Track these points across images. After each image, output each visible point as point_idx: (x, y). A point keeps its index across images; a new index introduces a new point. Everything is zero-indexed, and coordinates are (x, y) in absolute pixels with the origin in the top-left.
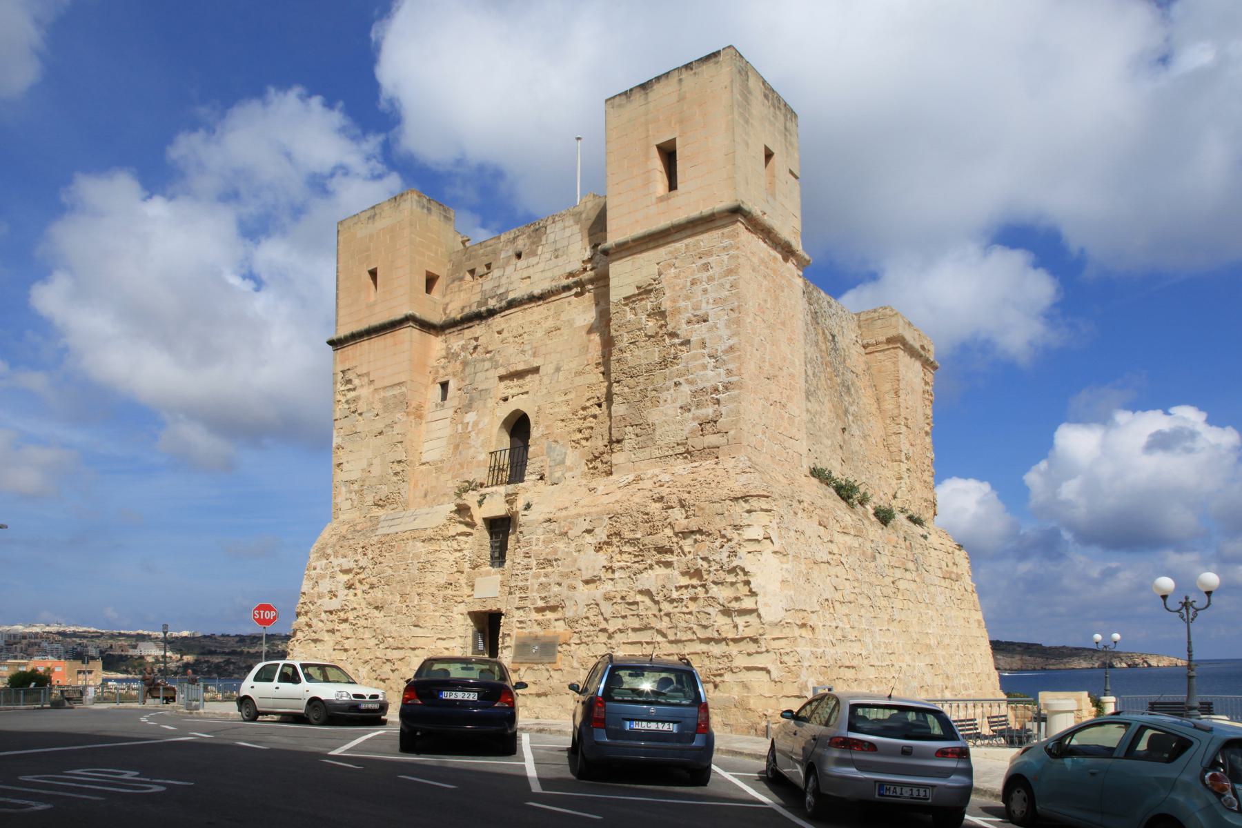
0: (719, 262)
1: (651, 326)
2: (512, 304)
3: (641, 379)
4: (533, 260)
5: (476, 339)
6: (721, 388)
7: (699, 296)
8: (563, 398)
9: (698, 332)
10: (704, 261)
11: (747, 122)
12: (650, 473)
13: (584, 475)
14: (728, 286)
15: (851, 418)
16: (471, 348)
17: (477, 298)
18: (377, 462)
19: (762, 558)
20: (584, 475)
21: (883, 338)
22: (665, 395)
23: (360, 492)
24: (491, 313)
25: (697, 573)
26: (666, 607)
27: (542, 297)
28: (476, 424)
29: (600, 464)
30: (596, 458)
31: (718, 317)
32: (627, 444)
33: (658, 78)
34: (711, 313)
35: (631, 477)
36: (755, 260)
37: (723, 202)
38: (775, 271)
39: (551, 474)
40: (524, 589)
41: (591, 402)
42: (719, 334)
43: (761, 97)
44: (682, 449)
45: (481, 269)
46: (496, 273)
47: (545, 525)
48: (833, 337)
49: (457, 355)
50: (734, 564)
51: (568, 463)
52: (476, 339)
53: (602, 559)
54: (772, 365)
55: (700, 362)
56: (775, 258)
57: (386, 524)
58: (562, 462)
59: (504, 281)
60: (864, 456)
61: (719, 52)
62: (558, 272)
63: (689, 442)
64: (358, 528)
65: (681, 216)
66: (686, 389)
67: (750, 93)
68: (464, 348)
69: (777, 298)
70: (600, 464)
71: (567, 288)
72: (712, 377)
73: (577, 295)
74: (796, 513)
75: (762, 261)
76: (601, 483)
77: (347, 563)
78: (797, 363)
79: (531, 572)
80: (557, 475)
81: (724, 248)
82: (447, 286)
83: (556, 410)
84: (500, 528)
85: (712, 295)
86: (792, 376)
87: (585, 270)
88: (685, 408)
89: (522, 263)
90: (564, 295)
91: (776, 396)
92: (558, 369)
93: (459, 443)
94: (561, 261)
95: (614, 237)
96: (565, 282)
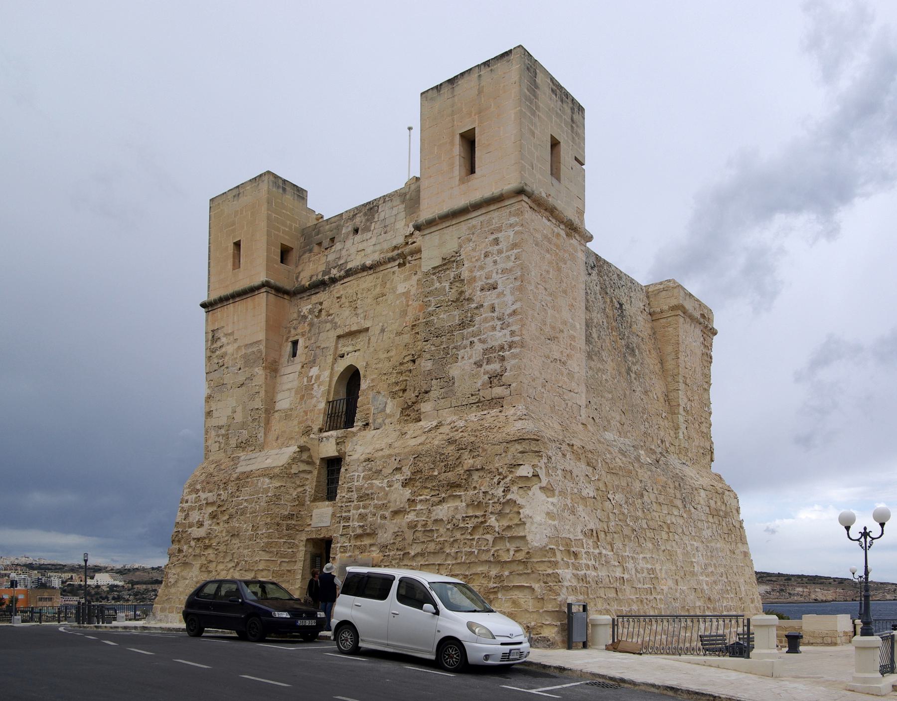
0: (507, 236)
2: (349, 273)
3: (444, 339)
4: (369, 234)
5: (321, 304)
6: (506, 347)
7: (490, 267)
8: (385, 355)
9: (490, 298)
10: (494, 236)
11: (534, 114)
12: (449, 420)
13: (399, 421)
14: (513, 258)
15: (633, 375)
16: (317, 311)
17: (322, 268)
18: (239, 409)
19: (530, 493)
20: (399, 421)
21: (666, 307)
22: (461, 353)
23: (226, 437)
24: (334, 281)
27: (371, 268)
28: (318, 377)
29: (410, 412)
30: (409, 407)
31: (505, 285)
32: (433, 394)
33: (462, 74)
34: (500, 282)
35: (435, 423)
36: (539, 236)
37: (512, 184)
38: (557, 246)
39: (374, 420)
40: (347, 519)
41: (407, 359)
42: (506, 299)
43: (548, 91)
44: (474, 399)
45: (326, 243)
46: (338, 246)
47: (365, 464)
48: (621, 305)
49: (305, 317)
50: (508, 497)
51: (388, 411)
52: (321, 304)
53: (407, 493)
54: (553, 328)
55: (490, 324)
56: (558, 235)
57: (244, 463)
58: (384, 410)
59: (344, 253)
60: (644, 409)
61: (510, 51)
62: (386, 246)
63: (481, 393)
64: (222, 467)
65: (477, 196)
66: (479, 347)
67: (537, 87)
68: (311, 311)
69: (559, 270)
70: (410, 412)
71: (392, 259)
72: (500, 337)
73: (400, 265)
74: (564, 455)
75: (545, 237)
76: (412, 429)
77: (211, 497)
78: (578, 326)
79: (353, 504)
80: (380, 421)
81: (511, 225)
82: (300, 257)
83: (380, 365)
84: (333, 465)
85: (501, 266)
86: (573, 338)
87: (407, 243)
88: (478, 364)
89: (358, 237)
90: (389, 265)
91: (557, 355)
92: (383, 331)
94: (388, 236)
95: (426, 213)
96: (390, 255)
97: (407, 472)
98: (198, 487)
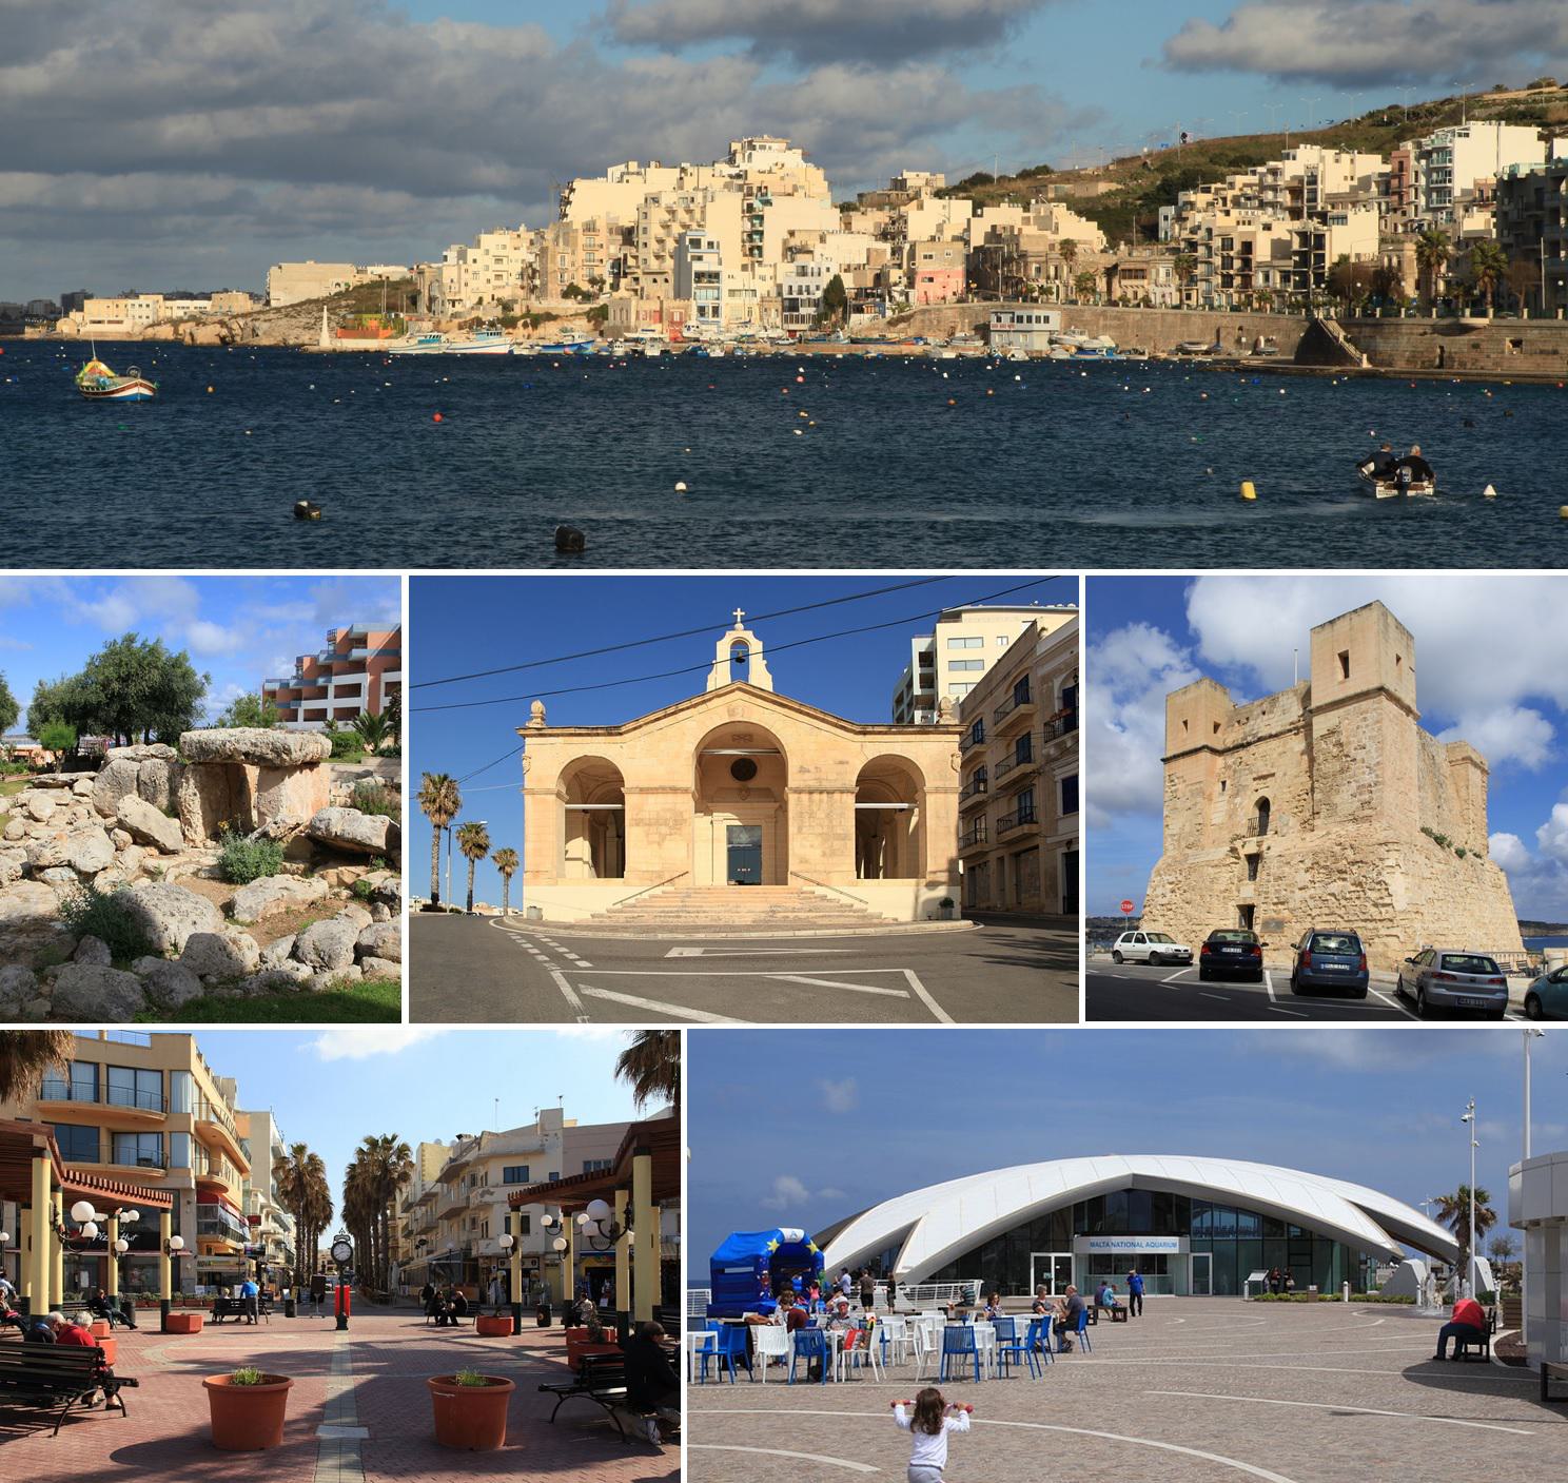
1: (1335, 751)
9: (1360, 755)
25: (1360, 884)
26: (1343, 902)
46: (1251, 722)
53: (1308, 876)
88: (1353, 796)
93: (1231, 814)
97: (1308, 863)
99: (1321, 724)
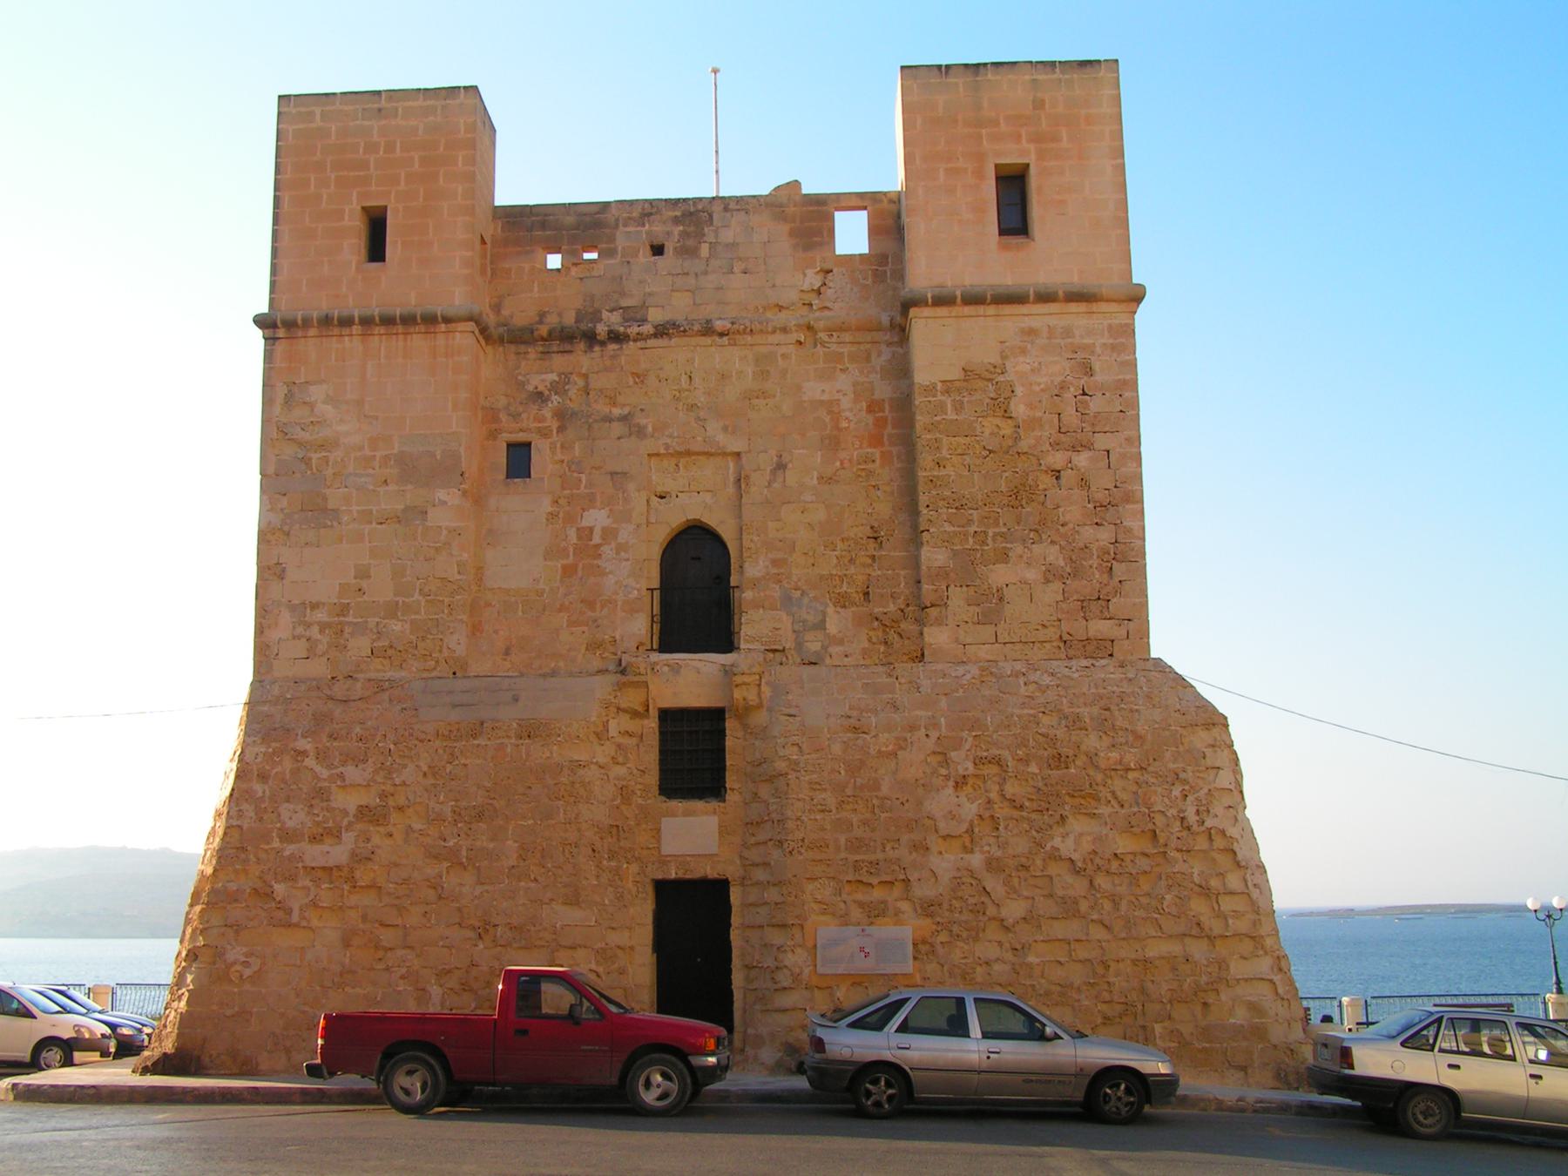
28: (609, 534)
58: (821, 625)
89: (667, 262)
92: (781, 467)
98: (303, 744)
99: (938, 347)
